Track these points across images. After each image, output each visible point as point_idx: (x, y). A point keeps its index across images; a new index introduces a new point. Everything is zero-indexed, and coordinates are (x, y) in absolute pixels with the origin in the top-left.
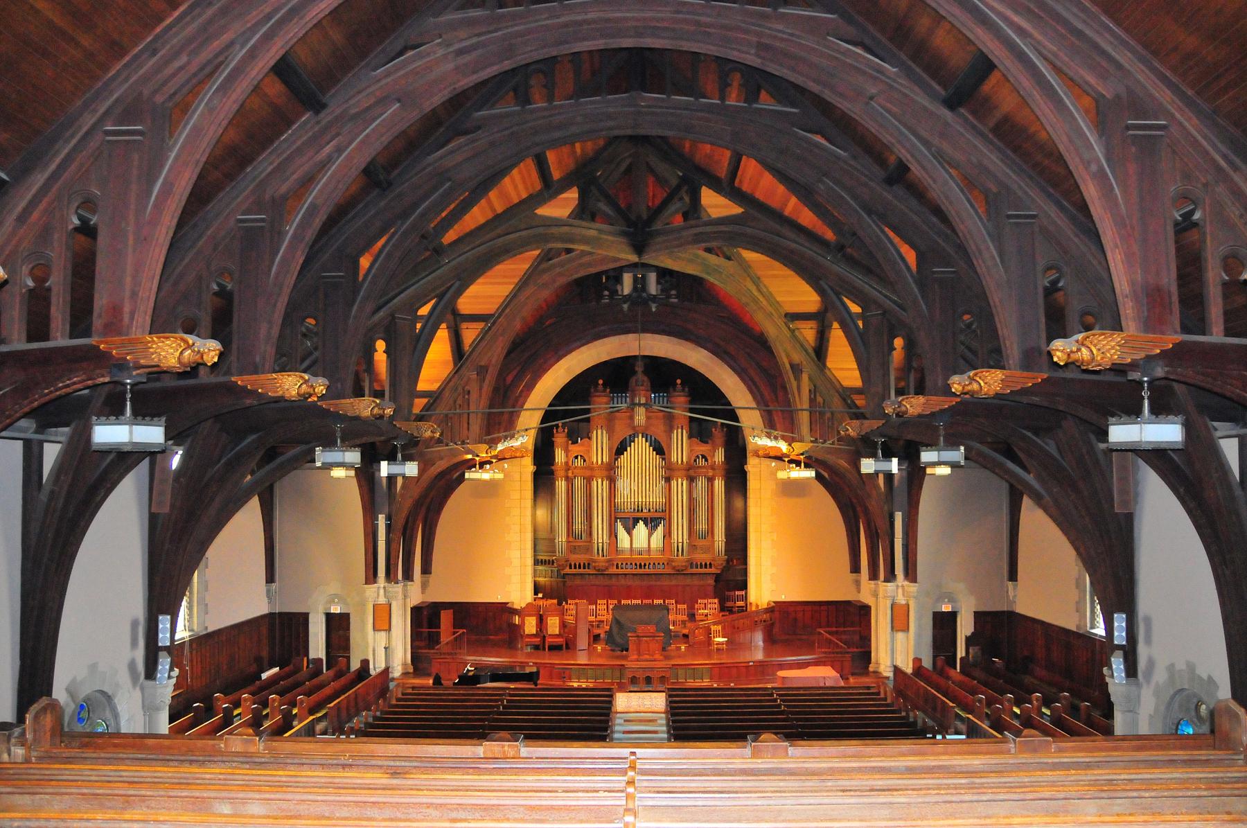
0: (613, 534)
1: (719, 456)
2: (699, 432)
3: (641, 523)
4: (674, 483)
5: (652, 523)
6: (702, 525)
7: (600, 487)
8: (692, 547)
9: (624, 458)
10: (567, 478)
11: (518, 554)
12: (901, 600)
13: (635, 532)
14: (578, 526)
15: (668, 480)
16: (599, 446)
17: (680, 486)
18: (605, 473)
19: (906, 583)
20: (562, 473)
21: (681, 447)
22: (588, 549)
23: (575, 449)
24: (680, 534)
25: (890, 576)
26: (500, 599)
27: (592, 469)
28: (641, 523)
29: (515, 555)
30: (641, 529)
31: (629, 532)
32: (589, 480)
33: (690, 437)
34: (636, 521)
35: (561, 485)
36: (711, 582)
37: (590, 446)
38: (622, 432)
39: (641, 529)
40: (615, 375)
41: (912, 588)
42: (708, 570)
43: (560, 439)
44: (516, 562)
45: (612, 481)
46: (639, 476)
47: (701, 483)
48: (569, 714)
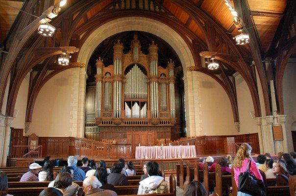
0: (155, 168)
1: (172, 73)
2: (162, 64)
3: (136, 103)
4: (152, 85)
5: (141, 105)
6: (164, 105)
7: (117, 85)
8: (161, 115)
9: (129, 74)
10: (102, 82)
11: (76, 113)
12: (276, 124)
13: (133, 108)
14: (107, 104)
15: (149, 84)
16: (117, 68)
17: (154, 86)
18: (120, 79)
19: (278, 116)
20: (100, 79)
21: (154, 69)
22: (111, 115)
23: (107, 69)
24: (155, 108)
25: (270, 112)
26: (66, 135)
27: (113, 77)
28: (136, 104)
29: (75, 113)
30: (136, 107)
31: (130, 108)
32: (112, 83)
33: (159, 65)
34: (134, 103)
35: (99, 85)
36: (169, 129)
37: (114, 68)
38: (128, 63)
39: (136, 107)
40: (126, 39)
41: (283, 118)
42: (167, 125)
43: (99, 63)
44: (76, 117)
45: (123, 83)
46: (135, 83)
47: (164, 86)
48: (13, 173)
